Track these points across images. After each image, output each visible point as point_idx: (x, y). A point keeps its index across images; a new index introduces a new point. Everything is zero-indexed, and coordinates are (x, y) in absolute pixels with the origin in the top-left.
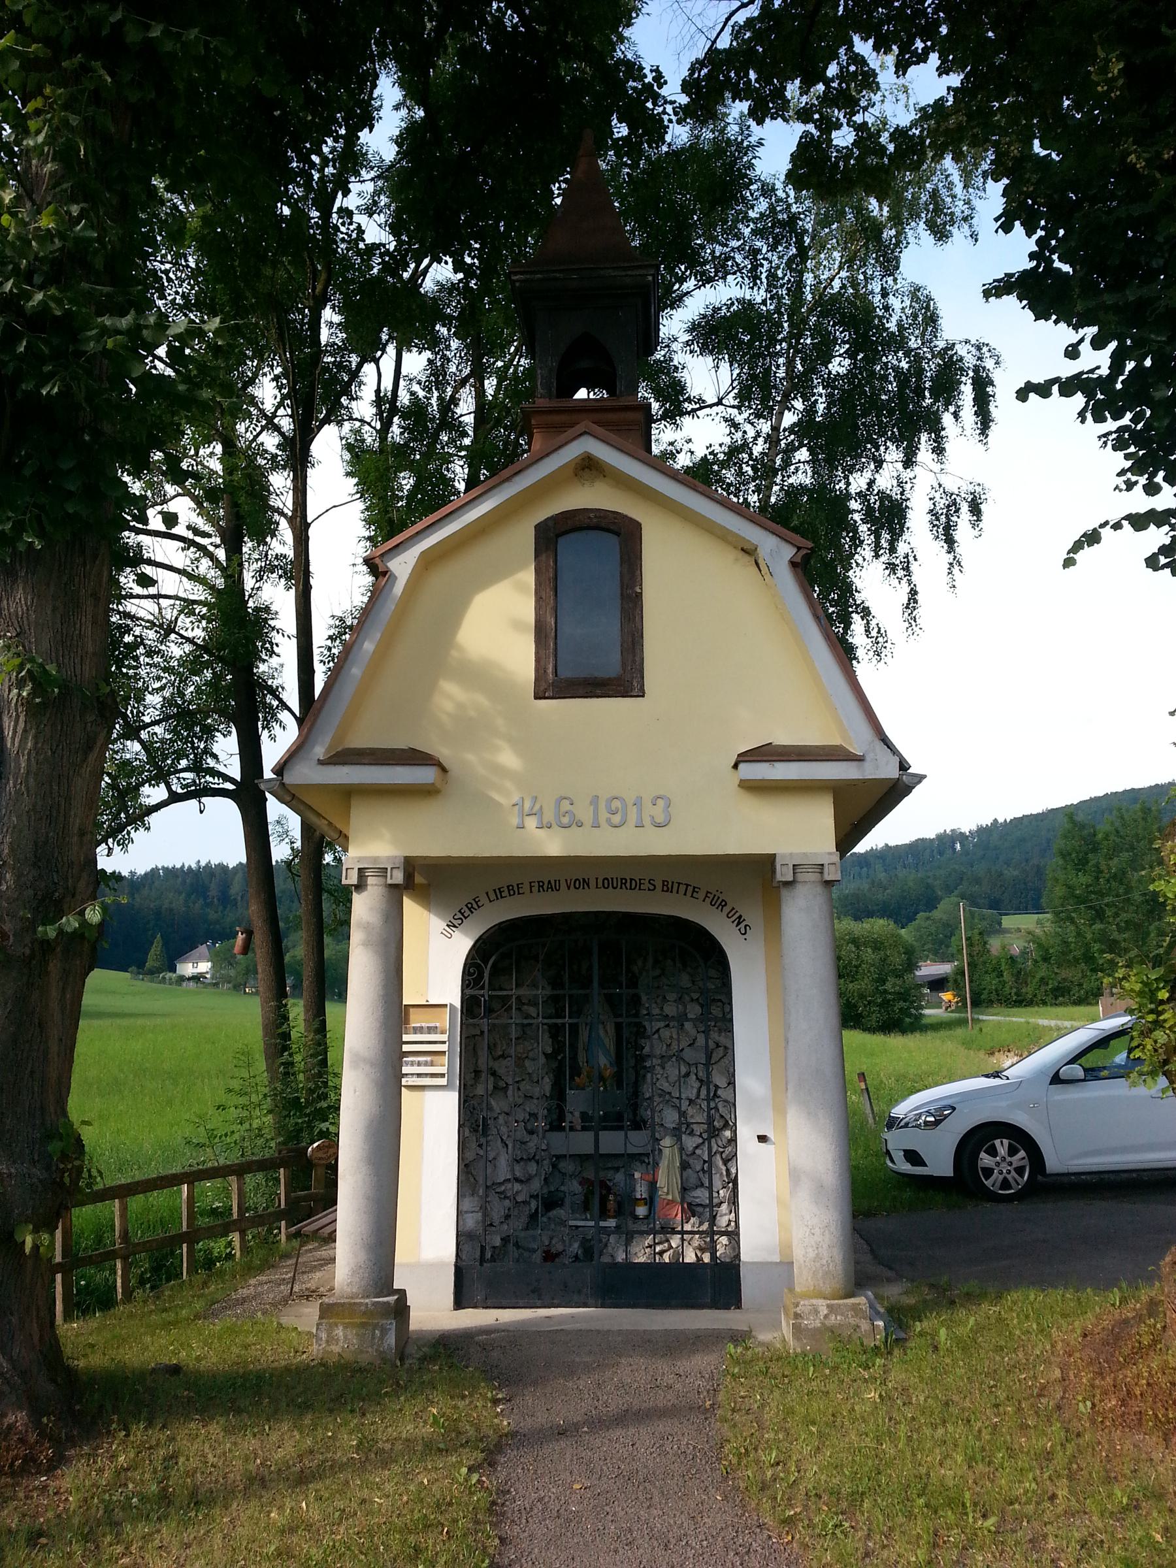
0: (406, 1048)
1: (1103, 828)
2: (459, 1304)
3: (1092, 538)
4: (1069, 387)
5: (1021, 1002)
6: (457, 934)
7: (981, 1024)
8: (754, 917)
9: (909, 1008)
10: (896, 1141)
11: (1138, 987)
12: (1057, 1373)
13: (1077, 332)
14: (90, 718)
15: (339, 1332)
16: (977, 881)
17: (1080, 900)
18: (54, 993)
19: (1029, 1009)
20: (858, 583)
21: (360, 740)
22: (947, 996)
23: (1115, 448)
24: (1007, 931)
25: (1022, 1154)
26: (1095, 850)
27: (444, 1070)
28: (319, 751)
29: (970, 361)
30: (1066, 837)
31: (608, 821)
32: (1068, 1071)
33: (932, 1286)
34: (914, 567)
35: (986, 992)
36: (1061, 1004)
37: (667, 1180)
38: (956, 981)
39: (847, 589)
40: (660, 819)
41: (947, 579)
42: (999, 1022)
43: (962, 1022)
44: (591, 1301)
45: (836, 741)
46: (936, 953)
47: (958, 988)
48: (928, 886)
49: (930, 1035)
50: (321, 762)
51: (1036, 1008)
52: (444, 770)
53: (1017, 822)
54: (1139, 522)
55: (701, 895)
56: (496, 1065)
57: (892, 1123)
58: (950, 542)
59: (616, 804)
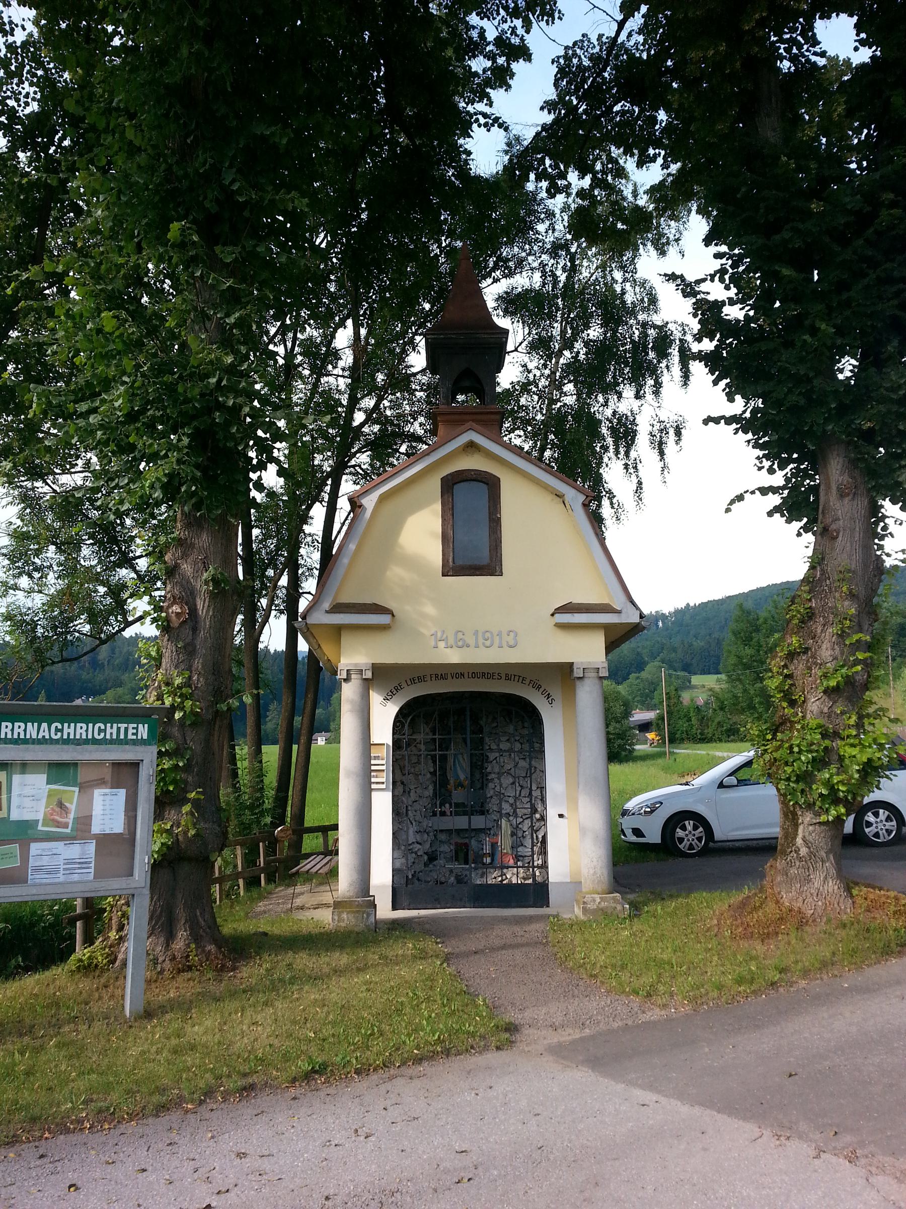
0: (373, 768)
1: (763, 614)
2: (394, 908)
3: (740, 498)
4: (729, 420)
5: (704, 739)
6: (389, 704)
7: (675, 756)
8: (556, 693)
9: (625, 744)
10: (627, 823)
11: (757, 733)
12: (715, 922)
13: (731, 399)
14: (235, 598)
15: (345, 916)
16: (674, 650)
17: (746, 667)
18: (216, 738)
19: (709, 745)
20: (605, 475)
21: (345, 599)
22: (651, 736)
23: (753, 447)
24: (695, 687)
25: (701, 829)
26: (757, 630)
27: (384, 780)
28: (326, 605)
29: (677, 335)
30: (737, 621)
31: (483, 644)
32: (727, 781)
33: (652, 893)
34: (639, 466)
35: (679, 732)
36: (732, 741)
37: (505, 842)
38: (658, 724)
39: (598, 480)
40: (512, 643)
41: (661, 478)
42: (688, 755)
43: (661, 755)
44: (467, 905)
45: (605, 601)
46: (643, 703)
47: (659, 729)
48: (638, 654)
49: (639, 764)
50: (327, 612)
51: (714, 744)
52: (393, 616)
53: (704, 605)
54: (764, 491)
55: (527, 682)
56: (404, 779)
57: (625, 813)
58: (662, 453)
59: (488, 635)
